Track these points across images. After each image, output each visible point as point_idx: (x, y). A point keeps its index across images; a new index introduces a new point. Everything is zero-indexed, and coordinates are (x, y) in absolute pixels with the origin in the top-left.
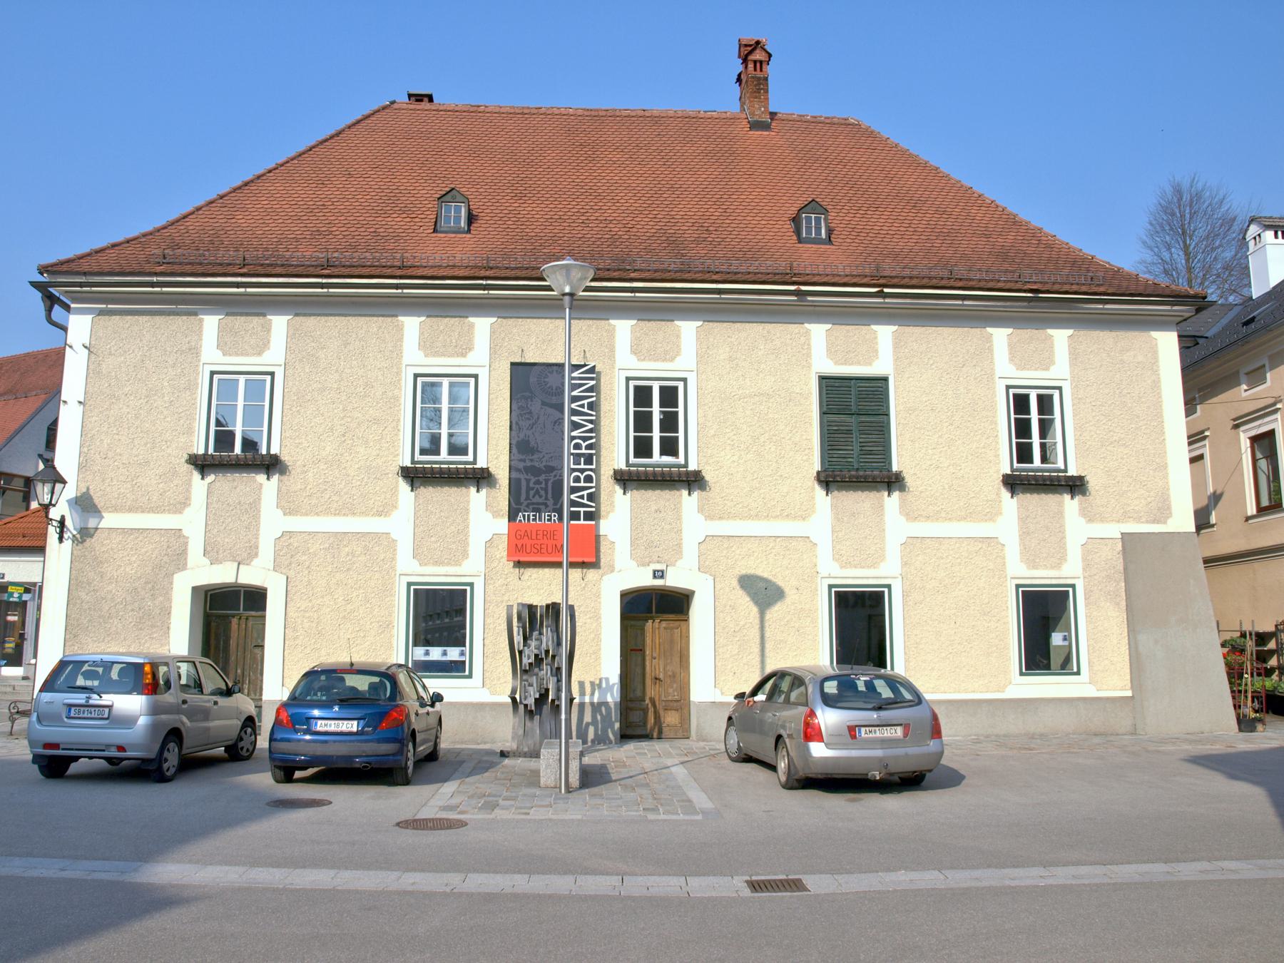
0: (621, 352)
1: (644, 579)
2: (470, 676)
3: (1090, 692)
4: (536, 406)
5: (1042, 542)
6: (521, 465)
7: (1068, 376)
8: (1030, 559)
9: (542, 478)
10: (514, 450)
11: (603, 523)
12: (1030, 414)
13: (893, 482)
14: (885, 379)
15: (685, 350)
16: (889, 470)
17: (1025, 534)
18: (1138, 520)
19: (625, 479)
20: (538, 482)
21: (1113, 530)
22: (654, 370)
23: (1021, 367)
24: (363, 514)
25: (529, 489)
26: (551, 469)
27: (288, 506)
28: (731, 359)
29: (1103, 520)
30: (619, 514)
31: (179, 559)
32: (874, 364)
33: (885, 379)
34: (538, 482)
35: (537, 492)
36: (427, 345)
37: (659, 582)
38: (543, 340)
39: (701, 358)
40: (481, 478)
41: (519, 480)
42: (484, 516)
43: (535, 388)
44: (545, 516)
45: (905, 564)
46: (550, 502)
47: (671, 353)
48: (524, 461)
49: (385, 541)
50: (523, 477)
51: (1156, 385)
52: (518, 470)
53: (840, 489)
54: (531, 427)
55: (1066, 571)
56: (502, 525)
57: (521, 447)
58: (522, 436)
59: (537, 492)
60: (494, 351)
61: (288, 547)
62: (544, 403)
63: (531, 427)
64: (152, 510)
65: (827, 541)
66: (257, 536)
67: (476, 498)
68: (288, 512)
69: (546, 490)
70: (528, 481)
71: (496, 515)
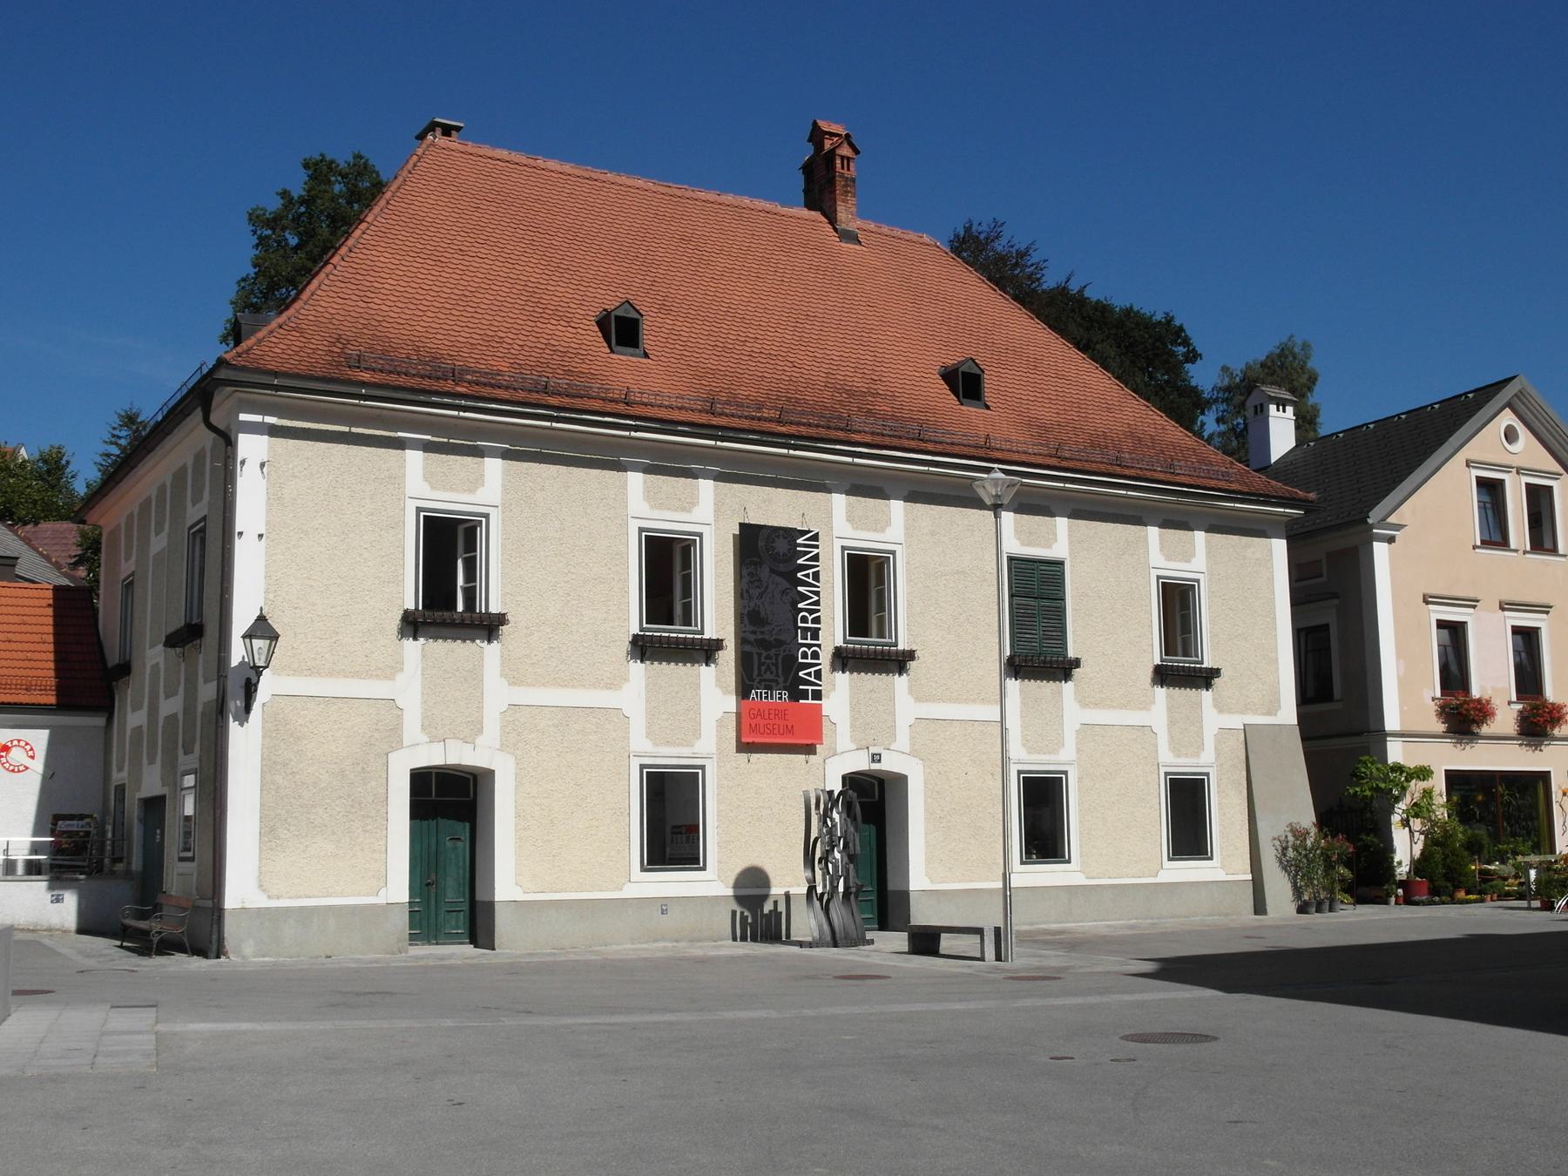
0: (838, 524)
1: (861, 763)
2: (704, 868)
3: (1079, 880)
4: (764, 573)
5: (1186, 732)
6: (752, 638)
7: (711, 519)
8: (1176, 748)
9: (773, 652)
10: (746, 621)
11: (824, 702)
12: (448, 544)
13: (489, 627)
14: (1061, 563)
15: (891, 526)
16: (1065, 656)
17: (1172, 723)
18: (1255, 712)
19: (844, 660)
20: (768, 657)
21: (1237, 721)
22: (867, 540)
23: (1168, 558)
24: (594, 686)
25: (761, 664)
26: (780, 643)
27: (514, 676)
28: (933, 534)
29: (1230, 711)
30: (840, 694)
31: (394, 737)
32: (479, 491)
33: (1061, 563)
34: (768, 657)
35: (768, 668)
36: (649, 495)
37: (875, 766)
38: (776, 507)
39: (908, 529)
40: (707, 651)
41: (750, 654)
42: (713, 691)
43: (768, 558)
44: (776, 693)
45: (1078, 750)
46: (781, 680)
47: (1188, 556)
48: (754, 632)
49: (617, 716)
50: (755, 650)
51: (1271, 580)
52: (750, 643)
53: (428, 636)
54: (761, 596)
55: (1202, 760)
56: (730, 703)
57: (749, 616)
58: (752, 605)
59: (768, 668)
60: (718, 511)
61: (517, 719)
62: (772, 571)
63: (761, 596)
64: (356, 675)
65: (1056, 728)
66: (480, 709)
67: (706, 673)
68: (515, 681)
69: (776, 665)
70: (760, 655)
71: (726, 692)
